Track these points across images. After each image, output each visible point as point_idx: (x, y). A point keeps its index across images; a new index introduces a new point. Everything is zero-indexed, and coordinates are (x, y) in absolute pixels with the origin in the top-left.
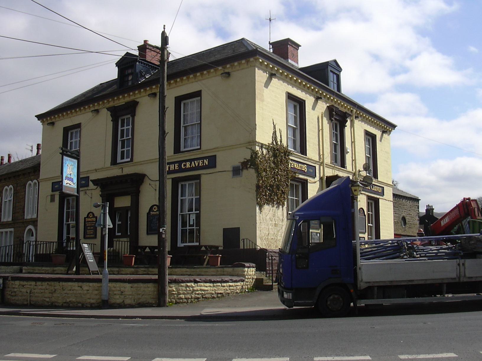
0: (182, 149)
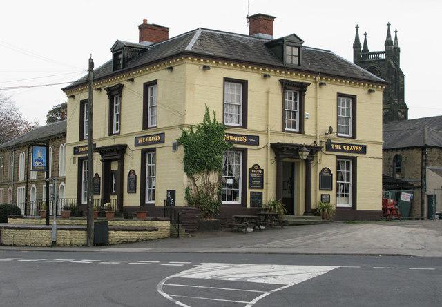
0: (150, 126)
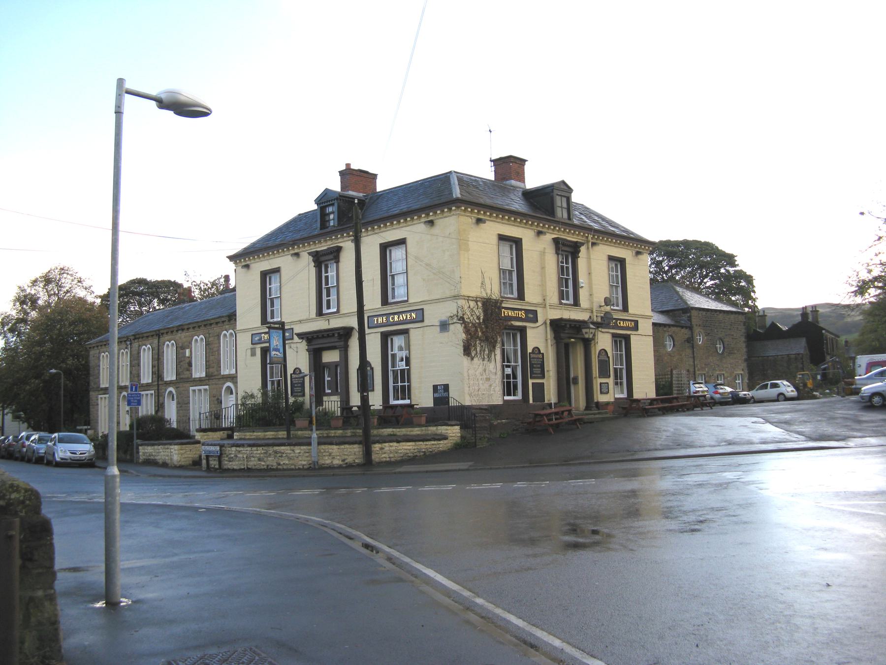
0: (390, 300)
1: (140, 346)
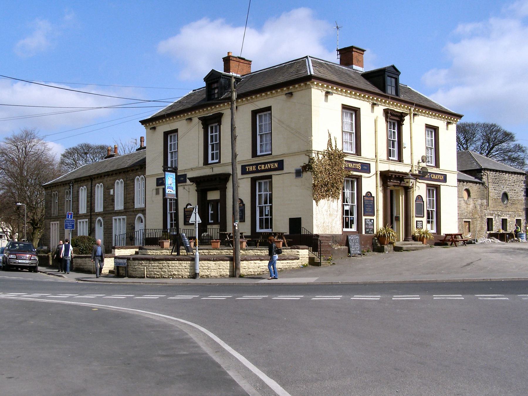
0: (259, 153)
1: (79, 187)
